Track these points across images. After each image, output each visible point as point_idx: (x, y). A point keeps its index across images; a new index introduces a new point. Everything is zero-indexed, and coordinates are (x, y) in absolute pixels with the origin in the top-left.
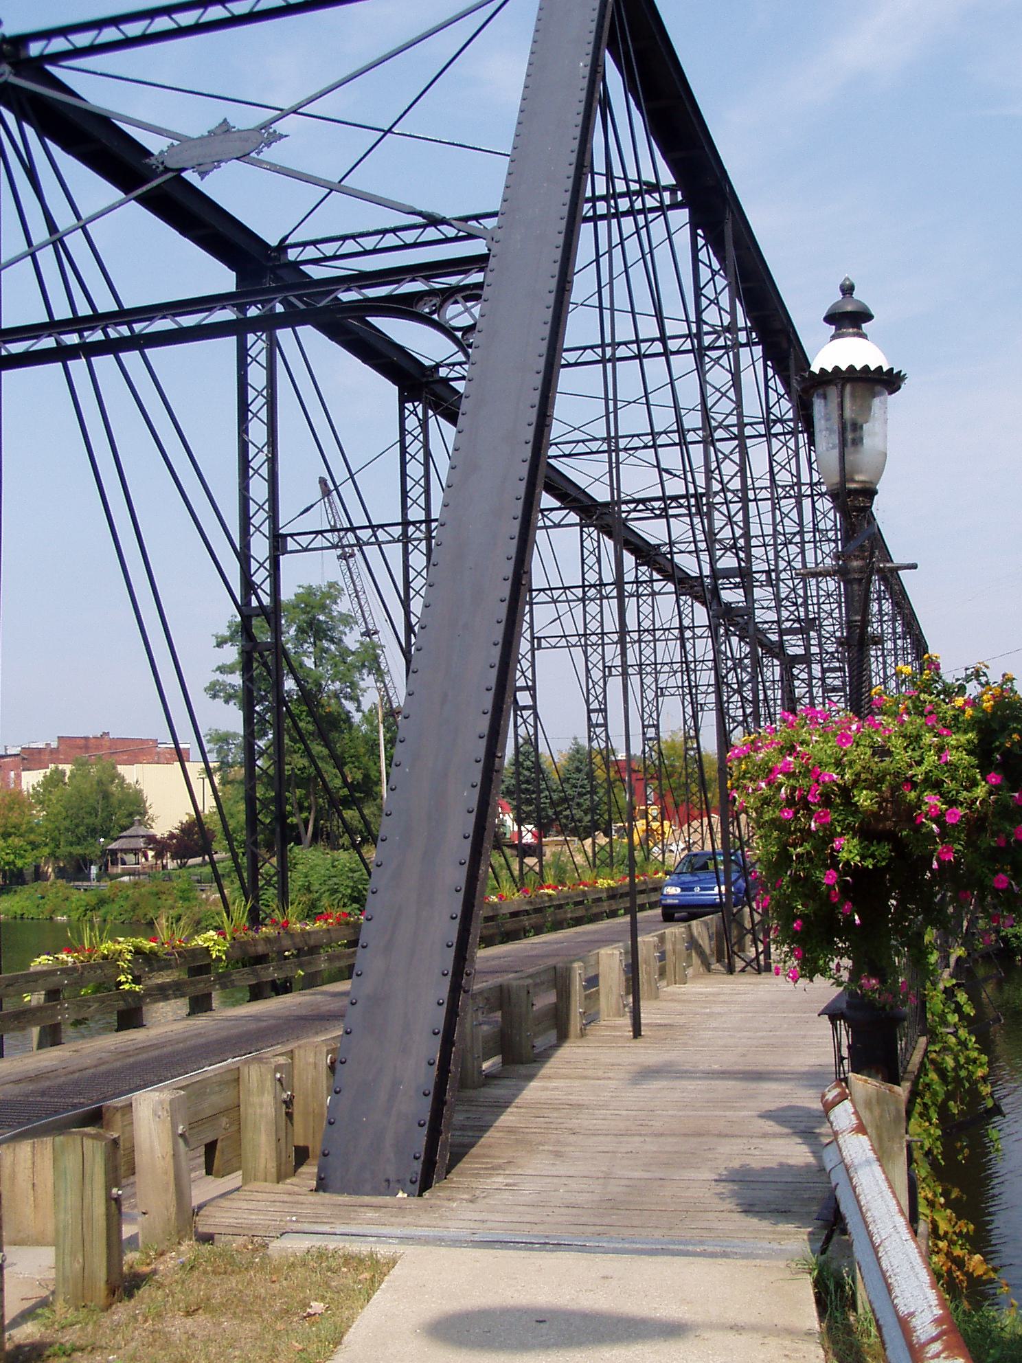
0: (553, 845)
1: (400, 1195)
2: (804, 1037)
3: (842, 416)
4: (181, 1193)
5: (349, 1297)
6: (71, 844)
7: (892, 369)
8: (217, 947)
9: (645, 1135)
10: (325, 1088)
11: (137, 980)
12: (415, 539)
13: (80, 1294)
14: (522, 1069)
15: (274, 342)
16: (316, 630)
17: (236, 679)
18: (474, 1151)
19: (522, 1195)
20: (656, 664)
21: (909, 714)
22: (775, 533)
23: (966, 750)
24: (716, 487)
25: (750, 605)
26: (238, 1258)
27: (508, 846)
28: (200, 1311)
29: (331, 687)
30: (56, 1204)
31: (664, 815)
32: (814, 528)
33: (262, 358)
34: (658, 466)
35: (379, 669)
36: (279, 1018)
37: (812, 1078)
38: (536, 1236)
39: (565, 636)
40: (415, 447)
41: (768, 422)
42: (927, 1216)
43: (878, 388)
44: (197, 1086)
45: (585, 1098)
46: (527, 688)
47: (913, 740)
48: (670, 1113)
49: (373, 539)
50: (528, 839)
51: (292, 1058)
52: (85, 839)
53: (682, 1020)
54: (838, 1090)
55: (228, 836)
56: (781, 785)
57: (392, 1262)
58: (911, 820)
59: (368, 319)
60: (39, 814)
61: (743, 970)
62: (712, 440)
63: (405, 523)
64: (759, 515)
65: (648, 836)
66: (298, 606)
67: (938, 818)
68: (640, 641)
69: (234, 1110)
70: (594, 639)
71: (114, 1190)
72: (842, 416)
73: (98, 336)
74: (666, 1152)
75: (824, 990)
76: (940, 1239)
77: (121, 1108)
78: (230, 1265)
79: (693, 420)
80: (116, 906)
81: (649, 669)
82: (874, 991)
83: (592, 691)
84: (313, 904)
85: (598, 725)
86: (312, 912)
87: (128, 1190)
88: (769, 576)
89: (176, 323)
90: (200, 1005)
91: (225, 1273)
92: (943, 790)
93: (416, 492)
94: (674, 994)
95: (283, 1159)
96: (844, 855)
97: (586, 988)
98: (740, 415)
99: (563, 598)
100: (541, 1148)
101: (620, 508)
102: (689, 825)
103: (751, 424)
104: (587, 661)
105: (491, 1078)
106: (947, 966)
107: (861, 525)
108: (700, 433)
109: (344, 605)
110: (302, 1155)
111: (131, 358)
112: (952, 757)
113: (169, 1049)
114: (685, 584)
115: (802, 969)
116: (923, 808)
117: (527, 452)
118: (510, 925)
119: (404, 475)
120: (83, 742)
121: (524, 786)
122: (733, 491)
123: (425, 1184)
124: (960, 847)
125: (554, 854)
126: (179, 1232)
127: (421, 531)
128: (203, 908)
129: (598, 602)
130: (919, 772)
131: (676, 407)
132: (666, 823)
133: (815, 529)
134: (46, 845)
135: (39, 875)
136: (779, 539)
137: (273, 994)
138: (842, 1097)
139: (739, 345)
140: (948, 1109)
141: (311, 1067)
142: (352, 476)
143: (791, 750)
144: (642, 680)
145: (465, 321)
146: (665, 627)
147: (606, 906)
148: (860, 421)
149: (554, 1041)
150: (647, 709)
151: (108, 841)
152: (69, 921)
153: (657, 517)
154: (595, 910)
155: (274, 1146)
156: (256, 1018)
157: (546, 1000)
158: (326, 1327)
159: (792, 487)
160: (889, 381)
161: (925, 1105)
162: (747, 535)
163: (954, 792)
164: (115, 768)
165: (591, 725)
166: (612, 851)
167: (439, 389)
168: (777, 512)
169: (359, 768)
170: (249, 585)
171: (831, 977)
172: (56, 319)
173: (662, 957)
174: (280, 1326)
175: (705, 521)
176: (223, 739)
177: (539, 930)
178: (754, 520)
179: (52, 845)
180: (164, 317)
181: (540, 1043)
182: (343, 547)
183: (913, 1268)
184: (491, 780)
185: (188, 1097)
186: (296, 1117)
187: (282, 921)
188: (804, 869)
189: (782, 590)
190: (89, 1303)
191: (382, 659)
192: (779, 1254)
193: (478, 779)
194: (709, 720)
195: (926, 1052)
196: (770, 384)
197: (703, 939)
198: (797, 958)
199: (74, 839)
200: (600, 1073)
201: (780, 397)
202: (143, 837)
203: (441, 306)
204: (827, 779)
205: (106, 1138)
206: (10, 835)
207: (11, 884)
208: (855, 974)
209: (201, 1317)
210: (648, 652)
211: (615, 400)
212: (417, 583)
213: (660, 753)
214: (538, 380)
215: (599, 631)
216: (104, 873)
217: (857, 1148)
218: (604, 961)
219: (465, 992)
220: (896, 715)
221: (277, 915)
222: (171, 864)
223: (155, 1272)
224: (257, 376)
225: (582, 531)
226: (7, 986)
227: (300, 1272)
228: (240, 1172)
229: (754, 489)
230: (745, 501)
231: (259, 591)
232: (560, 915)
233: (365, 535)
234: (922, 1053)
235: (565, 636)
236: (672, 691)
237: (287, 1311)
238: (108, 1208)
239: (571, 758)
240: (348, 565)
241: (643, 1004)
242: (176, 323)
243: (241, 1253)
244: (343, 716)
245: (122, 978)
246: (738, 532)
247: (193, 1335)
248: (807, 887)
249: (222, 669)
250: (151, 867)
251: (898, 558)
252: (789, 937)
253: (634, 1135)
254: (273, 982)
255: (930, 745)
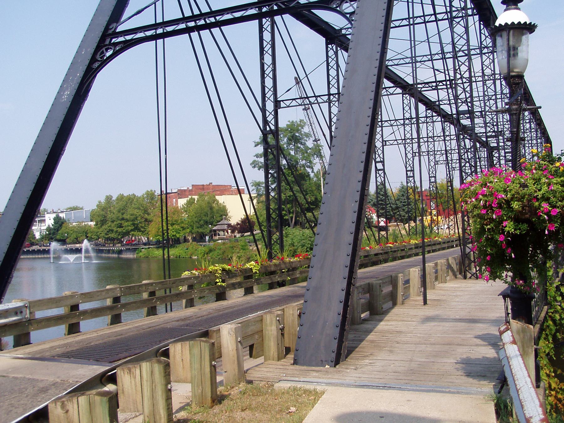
0: (392, 227)
1: (327, 366)
2: (495, 305)
3: (508, 44)
4: (240, 364)
5: (305, 406)
6: (198, 228)
7: (531, 23)
8: (255, 268)
9: (427, 344)
10: (297, 324)
11: (223, 281)
12: (334, 101)
13: (201, 401)
14: (377, 317)
15: (274, 22)
16: (295, 139)
17: (262, 160)
18: (357, 349)
19: (376, 367)
20: (434, 151)
21: (536, 170)
22: (484, 95)
23: (560, 185)
24: (458, 76)
25: (473, 126)
26: (262, 390)
27: (375, 227)
28: (247, 410)
29: (301, 163)
30: (191, 367)
31: (438, 214)
32: (501, 93)
33: (269, 29)
34: (433, 68)
35: (321, 155)
36: (280, 296)
37: (496, 322)
38: (380, 384)
39: (396, 140)
40: (333, 63)
41: (481, 48)
42: (546, 381)
43: (525, 31)
44: (246, 322)
45: (403, 329)
46: (381, 162)
47: (537, 181)
48: (438, 335)
49: (316, 102)
50: (382, 224)
51: (284, 312)
52: (203, 225)
53: (444, 298)
54: (506, 326)
55: (260, 225)
56: (481, 200)
57: (323, 393)
58: (536, 214)
59: (312, 10)
60: (185, 216)
61: (470, 278)
62: (456, 56)
63: (329, 95)
64: (477, 88)
65: (431, 223)
66: (287, 130)
67: (548, 214)
68: (428, 141)
69: (261, 332)
70: (408, 141)
71: (213, 363)
72: (508, 44)
73: (202, 22)
74: (435, 351)
75: (500, 285)
76: (552, 390)
77: (216, 331)
78: (259, 392)
79: (448, 48)
80: (216, 252)
81: (431, 153)
82: (522, 286)
83: (408, 163)
84: (295, 251)
85: (410, 177)
86: (294, 254)
87: (220, 363)
88: (482, 114)
89: (233, 16)
90: (249, 291)
91: (257, 395)
92: (550, 201)
93: (333, 82)
94: (441, 287)
95: (280, 352)
96: (507, 229)
97: (404, 284)
98: (468, 46)
99: (395, 124)
100: (384, 349)
101: (417, 86)
102: (449, 218)
103: (474, 49)
104: (406, 150)
105: (365, 320)
106: (558, 277)
107: (516, 91)
108: (451, 53)
109: (306, 129)
110: (288, 350)
111: (216, 31)
112: (554, 187)
113: (236, 309)
114: (446, 117)
115: (490, 276)
116: (541, 209)
117: (377, 64)
118: (375, 259)
119: (328, 75)
120: (202, 187)
121: (380, 202)
122: (466, 78)
123: (337, 362)
124: (558, 225)
125: (393, 230)
126: (239, 379)
127: (335, 98)
128: (251, 253)
129: (410, 125)
130: (540, 194)
131: (441, 43)
132: (440, 217)
133: (502, 93)
134: (188, 228)
135: (186, 240)
136: (486, 98)
137: (278, 287)
138: (507, 329)
139: (467, 15)
140: (557, 337)
141: (291, 316)
142: (307, 76)
143: (485, 185)
144: (429, 158)
145: (351, 10)
146: (438, 135)
147: (414, 251)
148: (516, 46)
149: (391, 306)
150: (431, 170)
151: (212, 226)
152: (198, 258)
153: (434, 89)
154: (409, 253)
155: (276, 347)
156: (271, 296)
157: (387, 289)
158: (296, 417)
159: (492, 75)
160: (529, 28)
161: (547, 334)
162: (471, 96)
163: (555, 202)
164: (215, 197)
165: (407, 177)
166: (416, 229)
167: (342, 39)
168: (485, 86)
169: (313, 196)
170: (266, 122)
171: (502, 280)
172: (185, 16)
173: (436, 272)
174: (278, 416)
175: (454, 91)
176: (257, 185)
177: (386, 261)
178: (475, 90)
179: (190, 228)
180: (228, 14)
181: (385, 306)
182: (305, 105)
183: (532, 399)
184: (363, 199)
185: (242, 327)
186: (286, 335)
187: (281, 257)
188: (491, 235)
189: (487, 119)
190: (204, 405)
191: (322, 151)
192: (481, 393)
193: (358, 198)
194: (456, 174)
195: (547, 313)
196: (482, 32)
197: (454, 265)
198: (488, 272)
199: (199, 226)
200: (410, 319)
201: (486, 37)
202: (226, 224)
203: (340, 4)
204: (500, 197)
205: (209, 342)
206: (174, 224)
207: (175, 244)
208: (513, 279)
209: (247, 412)
210: (431, 146)
211: (414, 41)
212: (334, 120)
213: (437, 188)
214: (381, 34)
215: (406, 138)
216: (211, 239)
217: (512, 350)
218: (411, 273)
219: (353, 285)
220: (531, 171)
221: (279, 255)
222: (238, 235)
223: (230, 394)
224: (267, 36)
225: (403, 96)
226: (173, 283)
227: (286, 396)
228: (263, 357)
229: (475, 77)
230: (471, 82)
231: (270, 124)
232: (395, 255)
233: (312, 100)
234: (545, 313)
235: (396, 140)
236: (441, 162)
237: (281, 411)
238: (211, 370)
239: (400, 191)
240: (307, 113)
241: (428, 292)
242: (233, 16)
243: (264, 388)
244: (307, 174)
245: (218, 280)
246: (468, 95)
247: (244, 418)
248: (491, 242)
249: (257, 156)
250: (230, 237)
251: (537, 105)
252: (488, 264)
253: (422, 344)
254: (278, 282)
255: (545, 183)
